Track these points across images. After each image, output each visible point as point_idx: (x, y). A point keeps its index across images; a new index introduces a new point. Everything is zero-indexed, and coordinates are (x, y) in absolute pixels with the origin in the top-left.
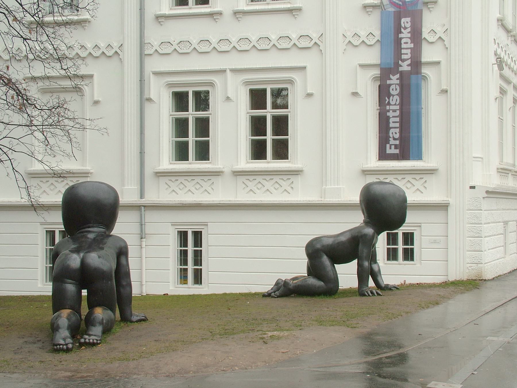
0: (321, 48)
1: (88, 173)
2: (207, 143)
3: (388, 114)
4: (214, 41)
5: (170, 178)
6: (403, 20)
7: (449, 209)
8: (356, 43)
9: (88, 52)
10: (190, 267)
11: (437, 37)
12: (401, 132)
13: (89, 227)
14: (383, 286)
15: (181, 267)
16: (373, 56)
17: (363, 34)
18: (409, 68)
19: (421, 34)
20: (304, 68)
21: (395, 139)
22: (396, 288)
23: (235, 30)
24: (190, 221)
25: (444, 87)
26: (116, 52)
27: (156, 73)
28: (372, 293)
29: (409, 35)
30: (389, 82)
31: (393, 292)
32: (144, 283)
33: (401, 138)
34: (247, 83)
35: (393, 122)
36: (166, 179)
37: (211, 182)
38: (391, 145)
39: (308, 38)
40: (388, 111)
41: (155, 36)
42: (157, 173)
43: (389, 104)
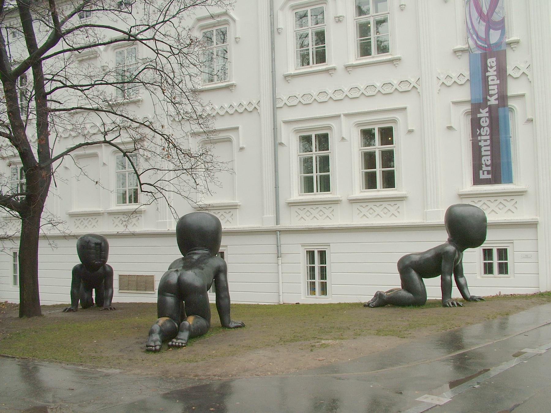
1: (237, 206)
3: (480, 144)
4: (330, 92)
6: (489, 60)
7: (538, 226)
8: (449, 83)
9: (234, 110)
10: (317, 280)
11: (521, 72)
14: (469, 297)
16: (464, 94)
17: (454, 75)
18: (497, 102)
19: (505, 71)
21: (487, 166)
22: (481, 299)
23: (345, 82)
24: (316, 242)
25: (530, 117)
26: (255, 108)
27: (285, 122)
28: (453, 304)
30: (479, 116)
31: (478, 303)
32: (281, 294)
33: (492, 165)
34: (358, 125)
35: (485, 151)
37: (331, 209)
38: (483, 171)
39: (407, 83)
40: (480, 141)
41: (284, 92)
42: (289, 203)
43: (480, 135)
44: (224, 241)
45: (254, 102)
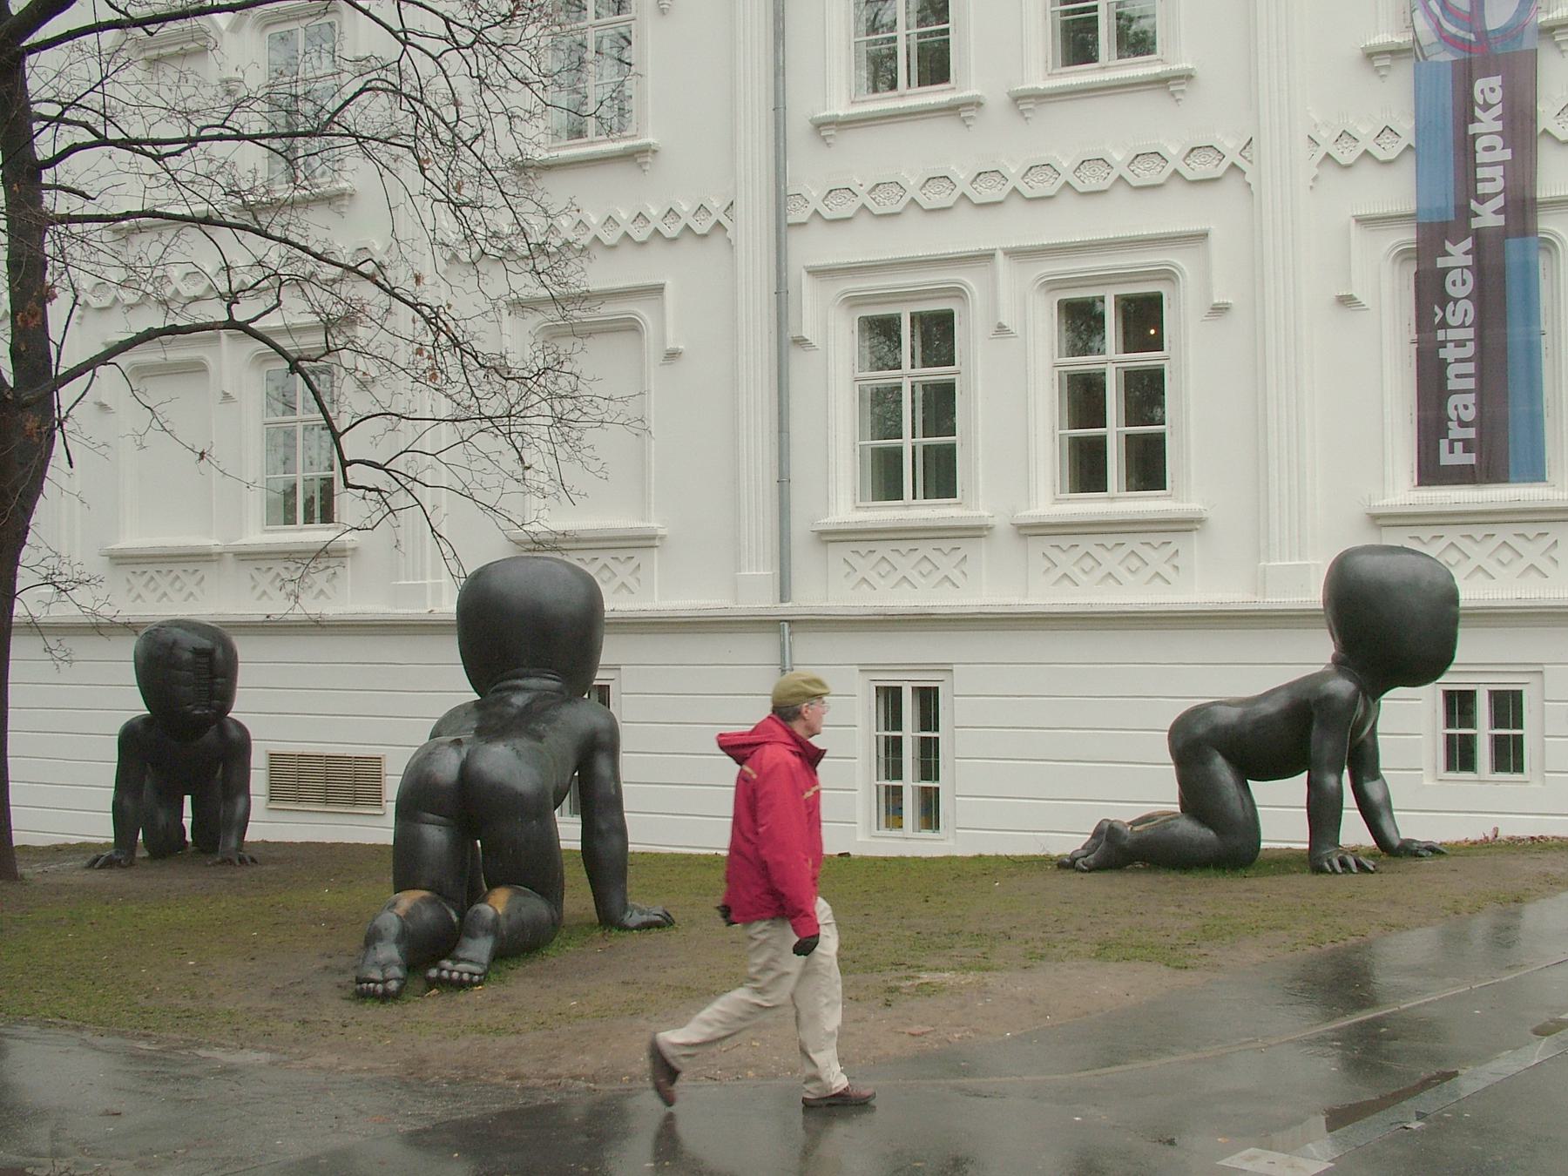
0: (1248, 178)
1: (654, 538)
2: (1158, 442)
3: (1443, 353)
5: (855, 547)
6: (1479, 85)
10: (910, 782)
12: (1480, 405)
13: (518, 677)
14: (1397, 843)
15: (888, 783)
16: (1395, 192)
17: (1365, 132)
18: (1500, 221)
19: (1534, 120)
20: (1204, 236)
21: (1463, 424)
22: (1434, 850)
23: (1011, 148)
24: (908, 660)
26: (718, 223)
27: (815, 272)
28: (1343, 863)
29: (1498, 126)
30: (1441, 262)
33: (1480, 422)
35: (1457, 376)
36: (844, 550)
37: (959, 555)
38: (1452, 442)
40: (1443, 344)
41: (812, 174)
43: (1444, 324)
44: (612, 651)
45: (685, 208)
